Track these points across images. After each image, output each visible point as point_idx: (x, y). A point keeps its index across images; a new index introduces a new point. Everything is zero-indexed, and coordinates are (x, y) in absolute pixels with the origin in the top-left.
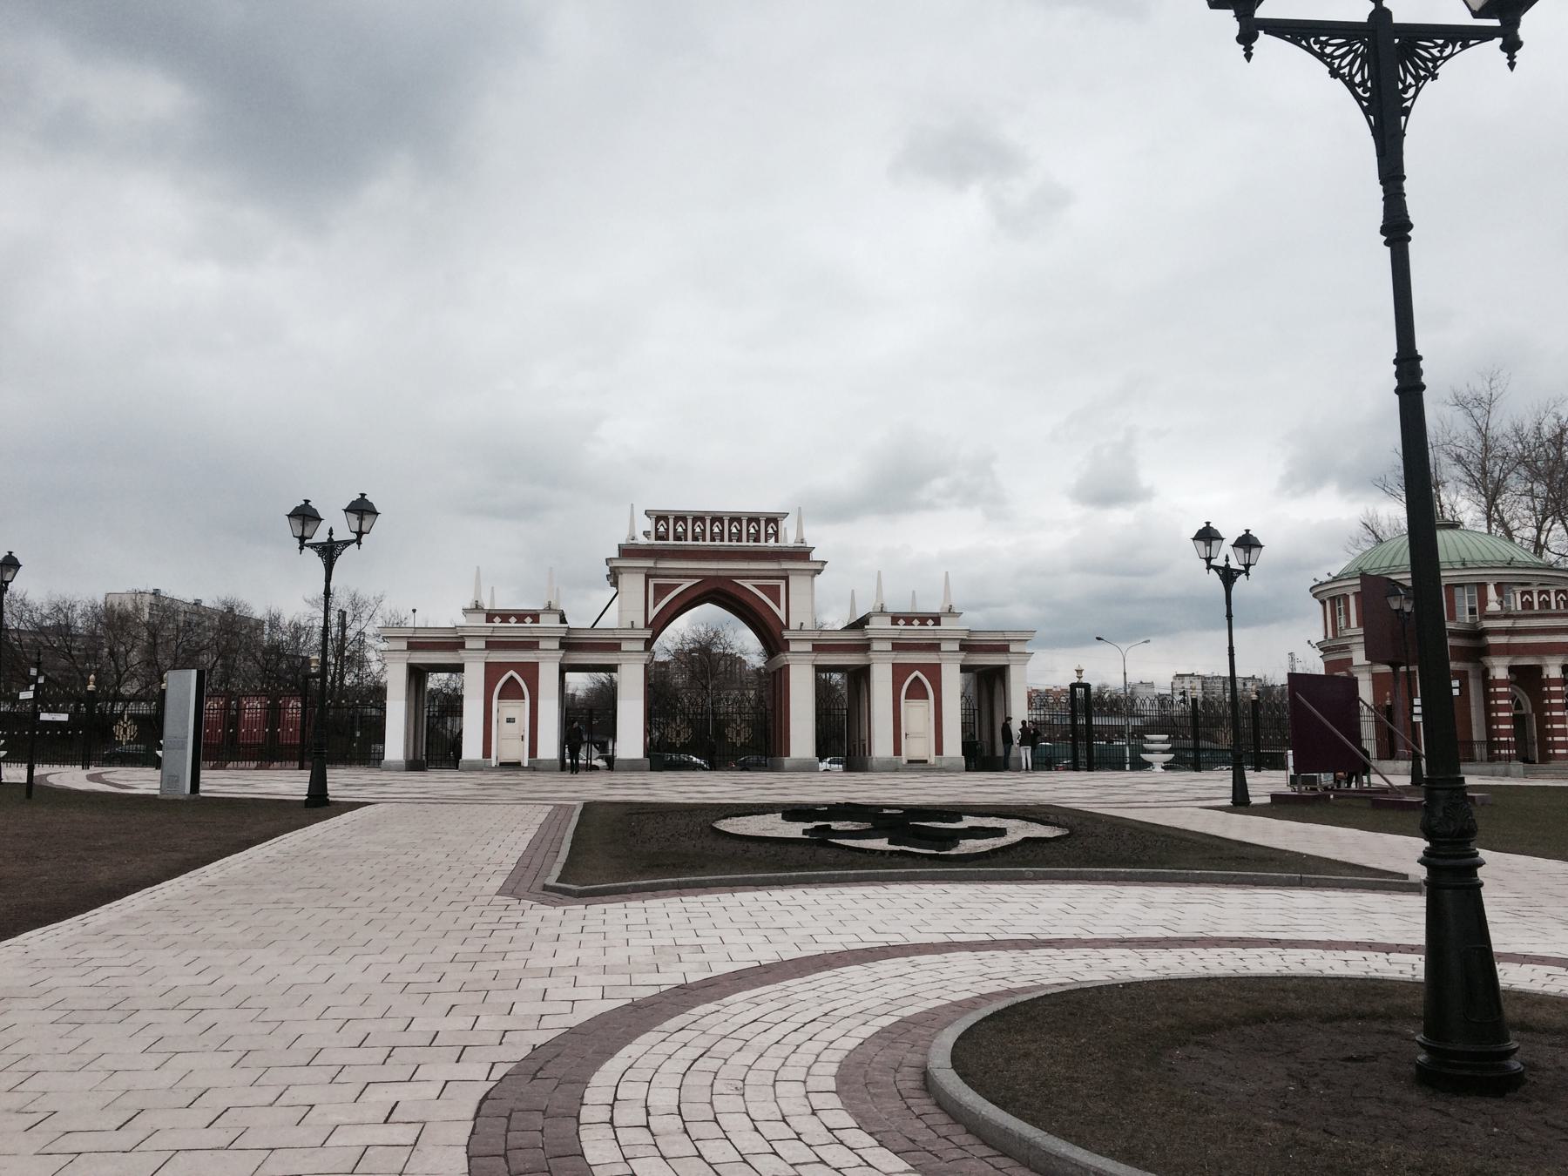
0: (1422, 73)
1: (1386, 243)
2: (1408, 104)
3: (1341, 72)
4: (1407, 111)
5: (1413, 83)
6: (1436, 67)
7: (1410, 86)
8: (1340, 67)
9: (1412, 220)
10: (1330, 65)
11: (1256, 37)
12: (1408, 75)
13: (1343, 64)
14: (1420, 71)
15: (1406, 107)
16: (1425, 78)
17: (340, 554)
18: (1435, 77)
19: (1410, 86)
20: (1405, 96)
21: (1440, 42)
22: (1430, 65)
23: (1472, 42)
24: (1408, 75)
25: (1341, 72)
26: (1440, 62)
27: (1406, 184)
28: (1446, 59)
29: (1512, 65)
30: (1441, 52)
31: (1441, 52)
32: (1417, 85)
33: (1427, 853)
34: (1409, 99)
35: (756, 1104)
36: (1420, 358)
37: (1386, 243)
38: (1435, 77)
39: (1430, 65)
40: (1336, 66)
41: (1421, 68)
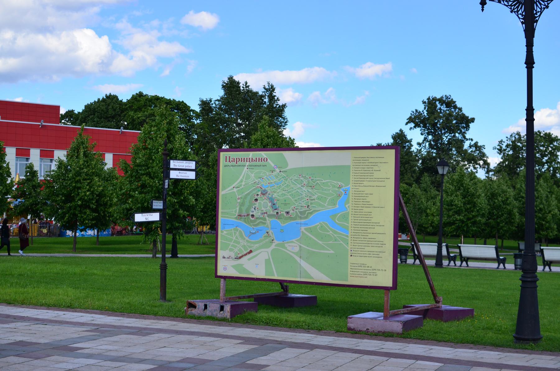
0: (513, 7)
1: (526, 67)
2: (502, 2)
3: (547, 5)
4: (537, 21)
5: (509, 4)
6: (515, 12)
7: (508, 3)
8: (545, 5)
9: (535, 61)
10: (544, 8)
11: (486, 4)
12: (512, 2)
13: (544, 4)
14: (513, 7)
15: (501, 2)
16: (511, 9)
17: (547, 7)
18: (511, 12)
19: (508, 3)
20: (505, 1)
21: (524, 14)
22: (516, 10)
23: (524, 25)
24: (512, 2)
25: (547, 5)
26: (517, 14)
27: (533, 47)
28: (518, 16)
29: (483, 10)
30: (520, 14)
31: (520, 14)
32: (509, 5)
33: (80, 113)
34: (504, 2)
35: (389, 300)
36: (526, 110)
37: (526, 67)
38: (511, 12)
39: (516, 10)
40: (545, 7)
41: (517, 9)
